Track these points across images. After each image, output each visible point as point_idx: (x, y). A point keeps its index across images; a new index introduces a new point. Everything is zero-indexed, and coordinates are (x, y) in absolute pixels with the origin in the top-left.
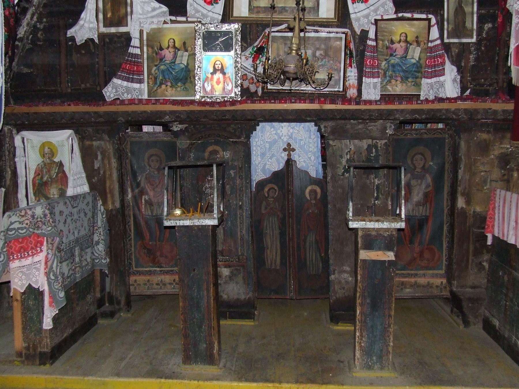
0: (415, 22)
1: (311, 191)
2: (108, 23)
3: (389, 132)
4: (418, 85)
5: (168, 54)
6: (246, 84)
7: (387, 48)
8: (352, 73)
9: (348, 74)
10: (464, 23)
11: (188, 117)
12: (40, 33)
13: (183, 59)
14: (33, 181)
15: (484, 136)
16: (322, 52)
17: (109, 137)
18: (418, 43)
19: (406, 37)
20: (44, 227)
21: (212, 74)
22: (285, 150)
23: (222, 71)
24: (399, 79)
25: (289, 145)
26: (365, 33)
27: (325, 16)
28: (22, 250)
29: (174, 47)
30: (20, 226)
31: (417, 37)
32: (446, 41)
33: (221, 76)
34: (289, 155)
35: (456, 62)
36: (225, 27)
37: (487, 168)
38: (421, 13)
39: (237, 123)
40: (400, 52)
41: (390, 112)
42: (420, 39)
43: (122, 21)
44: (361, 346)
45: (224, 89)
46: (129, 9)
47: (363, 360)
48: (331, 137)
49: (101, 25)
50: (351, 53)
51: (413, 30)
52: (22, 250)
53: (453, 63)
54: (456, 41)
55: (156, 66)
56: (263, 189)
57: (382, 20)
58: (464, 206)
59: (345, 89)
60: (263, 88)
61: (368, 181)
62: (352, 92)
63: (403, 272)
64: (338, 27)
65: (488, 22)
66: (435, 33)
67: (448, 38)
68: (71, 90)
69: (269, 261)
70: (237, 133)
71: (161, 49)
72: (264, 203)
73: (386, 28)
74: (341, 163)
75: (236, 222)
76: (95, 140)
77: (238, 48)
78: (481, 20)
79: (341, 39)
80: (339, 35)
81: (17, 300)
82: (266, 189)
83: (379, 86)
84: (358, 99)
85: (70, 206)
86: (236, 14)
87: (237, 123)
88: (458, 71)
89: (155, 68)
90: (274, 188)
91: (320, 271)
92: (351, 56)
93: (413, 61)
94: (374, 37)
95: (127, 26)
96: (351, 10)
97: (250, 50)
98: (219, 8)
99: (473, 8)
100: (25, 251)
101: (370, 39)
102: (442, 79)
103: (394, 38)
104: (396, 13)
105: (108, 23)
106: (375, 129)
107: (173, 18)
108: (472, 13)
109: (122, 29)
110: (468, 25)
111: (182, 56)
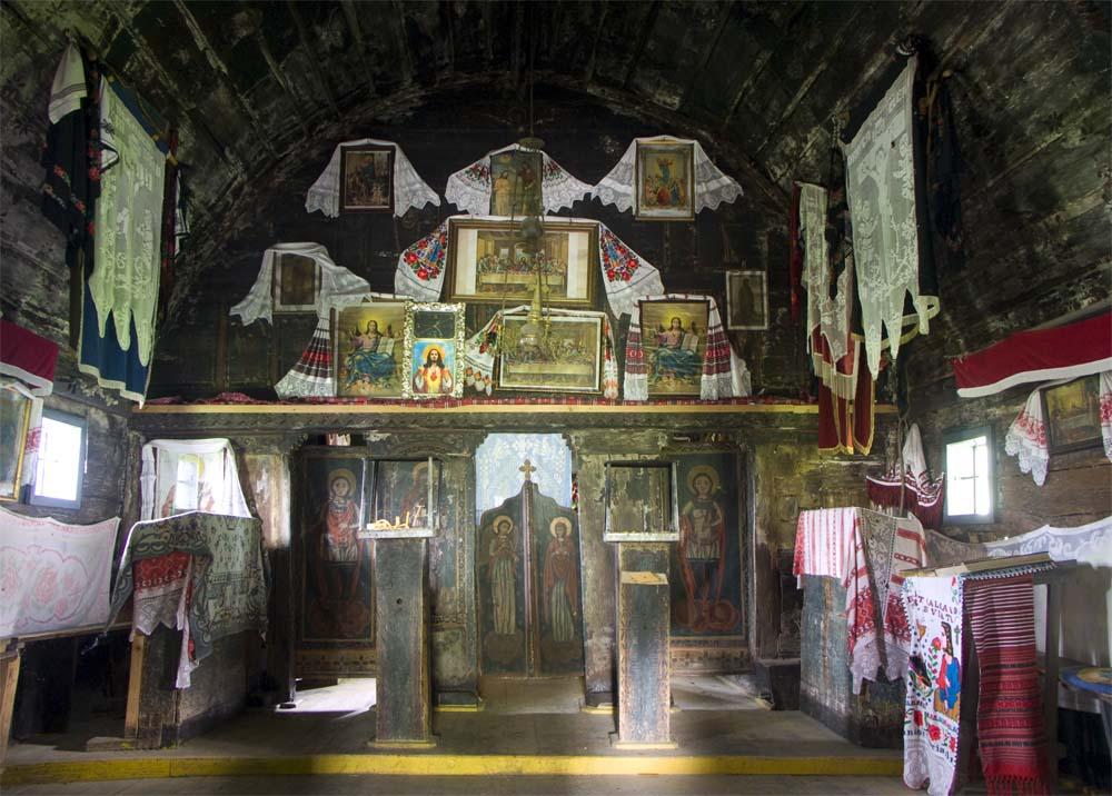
0: (691, 305)
1: (557, 526)
2: (288, 298)
3: (662, 444)
4: (697, 383)
5: (367, 342)
6: (471, 381)
7: (655, 336)
8: (611, 368)
9: (606, 368)
10: (753, 306)
11: (391, 422)
12: (192, 310)
13: (387, 347)
14: (164, 507)
15: (787, 449)
16: (571, 341)
17: (279, 449)
18: (695, 331)
19: (680, 323)
20: (192, 541)
21: (427, 366)
22: (522, 469)
23: (440, 363)
24: (672, 376)
25: (527, 462)
26: (626, 317)
27: (574, 296)
28: (155, 575)
29: (376, 331)
30: (157, 540)
31: (693, 324)
32: (730, 328)
33: (438, 369)
34: (528, 476)
35: (745, 354)
36: (444, 308)
37: (793, 490)
38: (698, 294)
39: (458, 433)
40: (672, 342)
41: (661, 417)
42: (697, 326)
43: (307, 297)
44: (626, 708)
45: (441, 386)
46: (317, 283)
47: (630, 727)
48: (585, 451)
49: (278, 302)
50: (609, 342)
51: (687, 314)
52: (155, 575)
53: (740, 355)
54: (743, 328)
55: (350, 355)
56: (492, 523)
57: (649, 302)
58: (766, 542)
59: (602, 387)
60: (493, 387)
61: (635, 509)
62: (611, 392)
63: (687, 638)
64: (591, 309)
65: (781, 306)
66: (715, 318)
67: (732, 325)
68: (231, 385)
69: (500, 625)
70: (458, 446)
71: (358, 334)
72: (493, 541)
73: (653, 312)
74: (598, 485)
75: (455, 565)
76: (260, 453)
77: (461, 334)
78: (773, 304)
79: (596, 324)
80: (592, 320)
81: (138, 648)
82: (496, 523)
83: (646, 383)
84: (620, 400)
85: (224, 526)
86: (459, 291)
87: (458, 433)
88: (747, 366)
89: (348, 359)
90: (505, 521)
91: (572, 636)
92: (609, 346)
93: (690, 353)
94: (638, 323)
95: (312, 303)
96: (608, 290)
97: (477, 336)
98: (437, 284)
99: (762, 289)
100: (159, 575)
101: (633, 325)
102: (728, 374)
103: (664, 324)
104: (665, 293)
105: (288, 298)
106: (642, 440)
107: (376, 295)
108: (762, 295)
109: (306, 308)
110: (757, 309)
111: (386, 344)
